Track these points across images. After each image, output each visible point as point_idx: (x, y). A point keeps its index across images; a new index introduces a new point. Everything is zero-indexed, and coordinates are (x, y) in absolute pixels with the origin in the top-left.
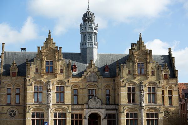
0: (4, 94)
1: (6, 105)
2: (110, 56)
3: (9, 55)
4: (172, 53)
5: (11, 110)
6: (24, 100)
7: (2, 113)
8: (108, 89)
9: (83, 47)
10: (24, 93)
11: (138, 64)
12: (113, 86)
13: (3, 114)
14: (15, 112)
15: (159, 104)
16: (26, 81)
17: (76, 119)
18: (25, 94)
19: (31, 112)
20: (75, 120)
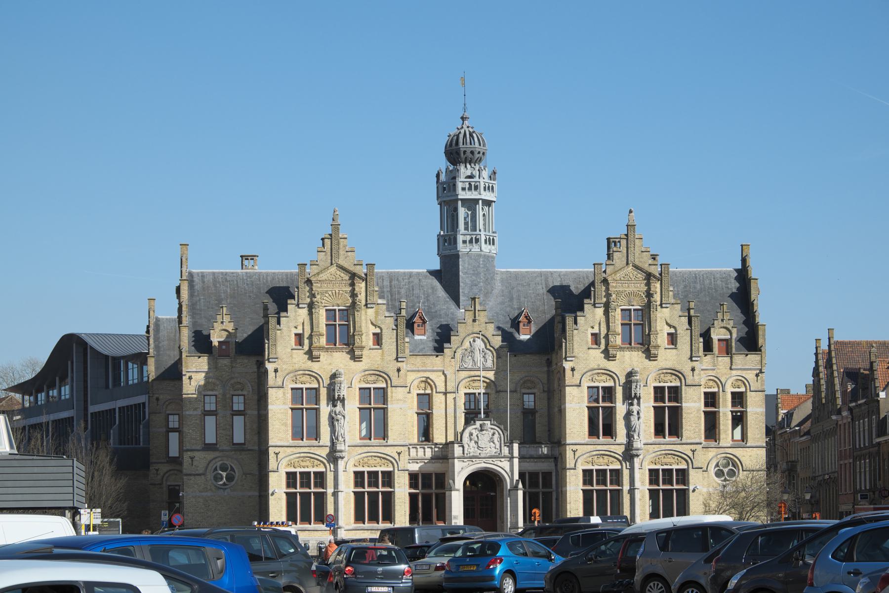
0: (195, 413)
1: (204, 449)
2: (538, 279)
3: (204, 282)
4: (751, 262)
5: (218, 464)
6: (259, 433)
7: (190, 475)
8: (529, 391)
9: (447, 252)
10: (259, 411)
11: (622, 310)
12: (545, 381)
13: (192, 477)
14: (232, 469)
15: (689, 441)
16: (263, 370)
17: (424, 491)
18: (262, 412)
19: (284, 469)
20: (544, 493)
